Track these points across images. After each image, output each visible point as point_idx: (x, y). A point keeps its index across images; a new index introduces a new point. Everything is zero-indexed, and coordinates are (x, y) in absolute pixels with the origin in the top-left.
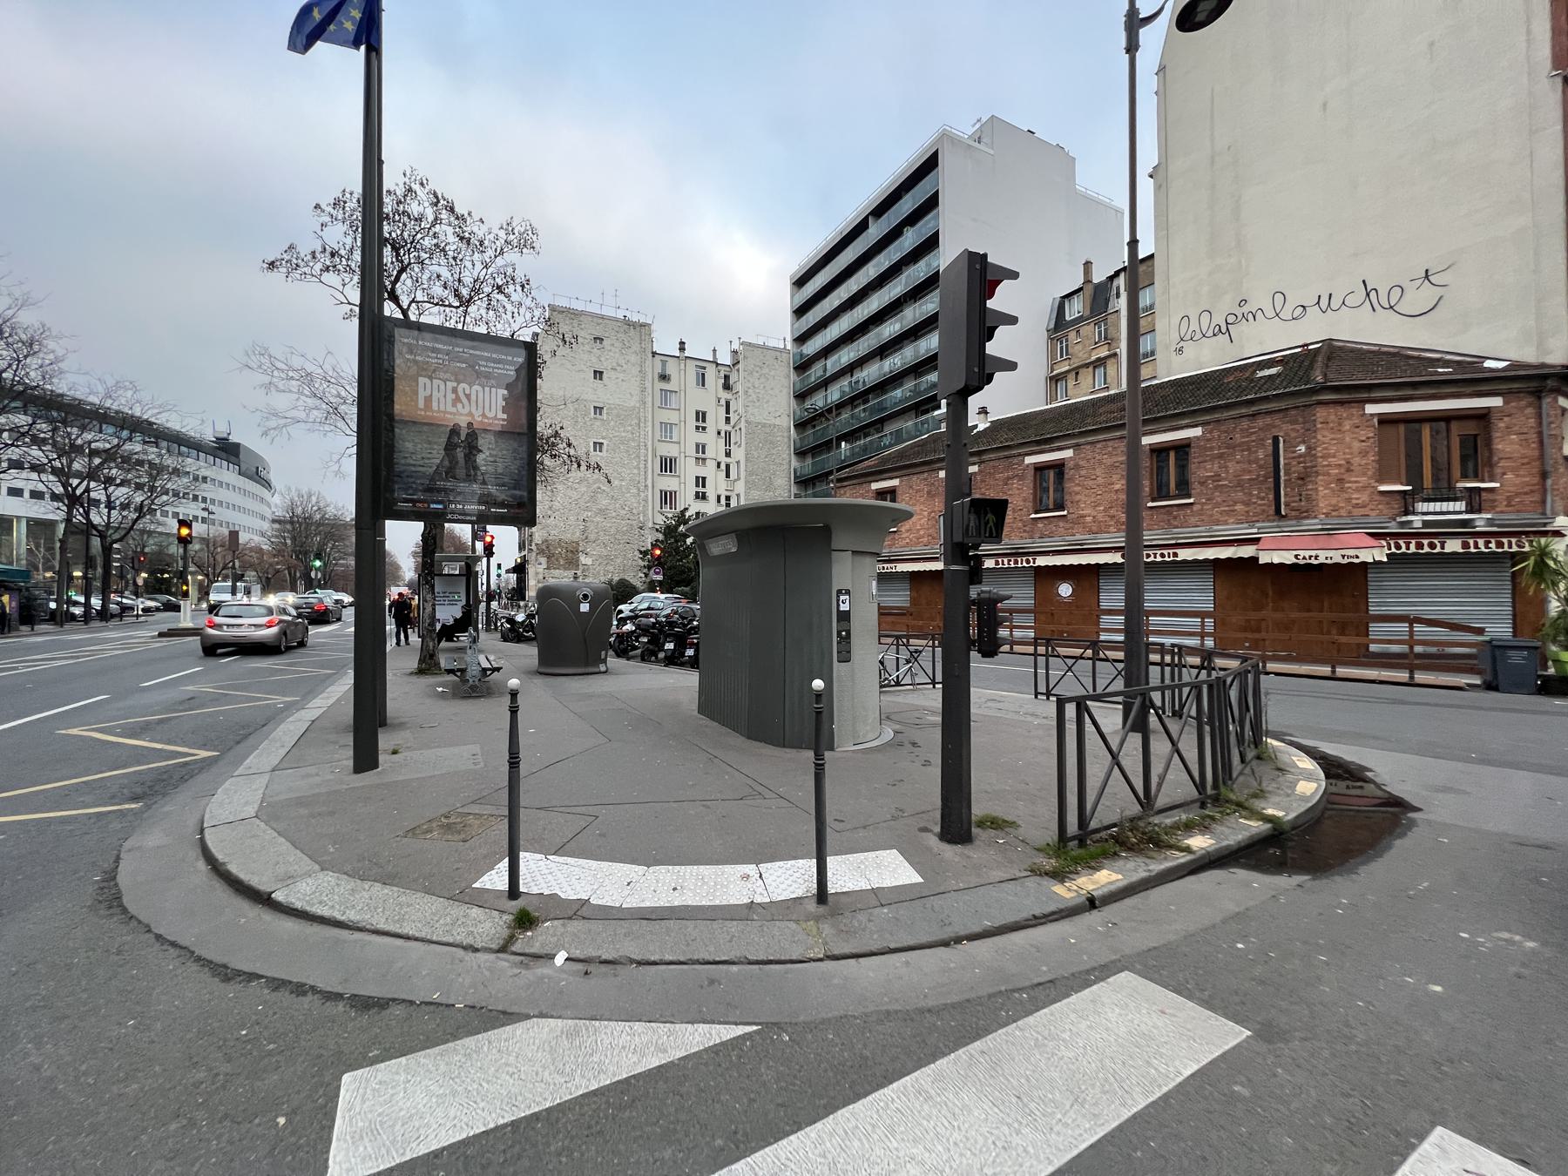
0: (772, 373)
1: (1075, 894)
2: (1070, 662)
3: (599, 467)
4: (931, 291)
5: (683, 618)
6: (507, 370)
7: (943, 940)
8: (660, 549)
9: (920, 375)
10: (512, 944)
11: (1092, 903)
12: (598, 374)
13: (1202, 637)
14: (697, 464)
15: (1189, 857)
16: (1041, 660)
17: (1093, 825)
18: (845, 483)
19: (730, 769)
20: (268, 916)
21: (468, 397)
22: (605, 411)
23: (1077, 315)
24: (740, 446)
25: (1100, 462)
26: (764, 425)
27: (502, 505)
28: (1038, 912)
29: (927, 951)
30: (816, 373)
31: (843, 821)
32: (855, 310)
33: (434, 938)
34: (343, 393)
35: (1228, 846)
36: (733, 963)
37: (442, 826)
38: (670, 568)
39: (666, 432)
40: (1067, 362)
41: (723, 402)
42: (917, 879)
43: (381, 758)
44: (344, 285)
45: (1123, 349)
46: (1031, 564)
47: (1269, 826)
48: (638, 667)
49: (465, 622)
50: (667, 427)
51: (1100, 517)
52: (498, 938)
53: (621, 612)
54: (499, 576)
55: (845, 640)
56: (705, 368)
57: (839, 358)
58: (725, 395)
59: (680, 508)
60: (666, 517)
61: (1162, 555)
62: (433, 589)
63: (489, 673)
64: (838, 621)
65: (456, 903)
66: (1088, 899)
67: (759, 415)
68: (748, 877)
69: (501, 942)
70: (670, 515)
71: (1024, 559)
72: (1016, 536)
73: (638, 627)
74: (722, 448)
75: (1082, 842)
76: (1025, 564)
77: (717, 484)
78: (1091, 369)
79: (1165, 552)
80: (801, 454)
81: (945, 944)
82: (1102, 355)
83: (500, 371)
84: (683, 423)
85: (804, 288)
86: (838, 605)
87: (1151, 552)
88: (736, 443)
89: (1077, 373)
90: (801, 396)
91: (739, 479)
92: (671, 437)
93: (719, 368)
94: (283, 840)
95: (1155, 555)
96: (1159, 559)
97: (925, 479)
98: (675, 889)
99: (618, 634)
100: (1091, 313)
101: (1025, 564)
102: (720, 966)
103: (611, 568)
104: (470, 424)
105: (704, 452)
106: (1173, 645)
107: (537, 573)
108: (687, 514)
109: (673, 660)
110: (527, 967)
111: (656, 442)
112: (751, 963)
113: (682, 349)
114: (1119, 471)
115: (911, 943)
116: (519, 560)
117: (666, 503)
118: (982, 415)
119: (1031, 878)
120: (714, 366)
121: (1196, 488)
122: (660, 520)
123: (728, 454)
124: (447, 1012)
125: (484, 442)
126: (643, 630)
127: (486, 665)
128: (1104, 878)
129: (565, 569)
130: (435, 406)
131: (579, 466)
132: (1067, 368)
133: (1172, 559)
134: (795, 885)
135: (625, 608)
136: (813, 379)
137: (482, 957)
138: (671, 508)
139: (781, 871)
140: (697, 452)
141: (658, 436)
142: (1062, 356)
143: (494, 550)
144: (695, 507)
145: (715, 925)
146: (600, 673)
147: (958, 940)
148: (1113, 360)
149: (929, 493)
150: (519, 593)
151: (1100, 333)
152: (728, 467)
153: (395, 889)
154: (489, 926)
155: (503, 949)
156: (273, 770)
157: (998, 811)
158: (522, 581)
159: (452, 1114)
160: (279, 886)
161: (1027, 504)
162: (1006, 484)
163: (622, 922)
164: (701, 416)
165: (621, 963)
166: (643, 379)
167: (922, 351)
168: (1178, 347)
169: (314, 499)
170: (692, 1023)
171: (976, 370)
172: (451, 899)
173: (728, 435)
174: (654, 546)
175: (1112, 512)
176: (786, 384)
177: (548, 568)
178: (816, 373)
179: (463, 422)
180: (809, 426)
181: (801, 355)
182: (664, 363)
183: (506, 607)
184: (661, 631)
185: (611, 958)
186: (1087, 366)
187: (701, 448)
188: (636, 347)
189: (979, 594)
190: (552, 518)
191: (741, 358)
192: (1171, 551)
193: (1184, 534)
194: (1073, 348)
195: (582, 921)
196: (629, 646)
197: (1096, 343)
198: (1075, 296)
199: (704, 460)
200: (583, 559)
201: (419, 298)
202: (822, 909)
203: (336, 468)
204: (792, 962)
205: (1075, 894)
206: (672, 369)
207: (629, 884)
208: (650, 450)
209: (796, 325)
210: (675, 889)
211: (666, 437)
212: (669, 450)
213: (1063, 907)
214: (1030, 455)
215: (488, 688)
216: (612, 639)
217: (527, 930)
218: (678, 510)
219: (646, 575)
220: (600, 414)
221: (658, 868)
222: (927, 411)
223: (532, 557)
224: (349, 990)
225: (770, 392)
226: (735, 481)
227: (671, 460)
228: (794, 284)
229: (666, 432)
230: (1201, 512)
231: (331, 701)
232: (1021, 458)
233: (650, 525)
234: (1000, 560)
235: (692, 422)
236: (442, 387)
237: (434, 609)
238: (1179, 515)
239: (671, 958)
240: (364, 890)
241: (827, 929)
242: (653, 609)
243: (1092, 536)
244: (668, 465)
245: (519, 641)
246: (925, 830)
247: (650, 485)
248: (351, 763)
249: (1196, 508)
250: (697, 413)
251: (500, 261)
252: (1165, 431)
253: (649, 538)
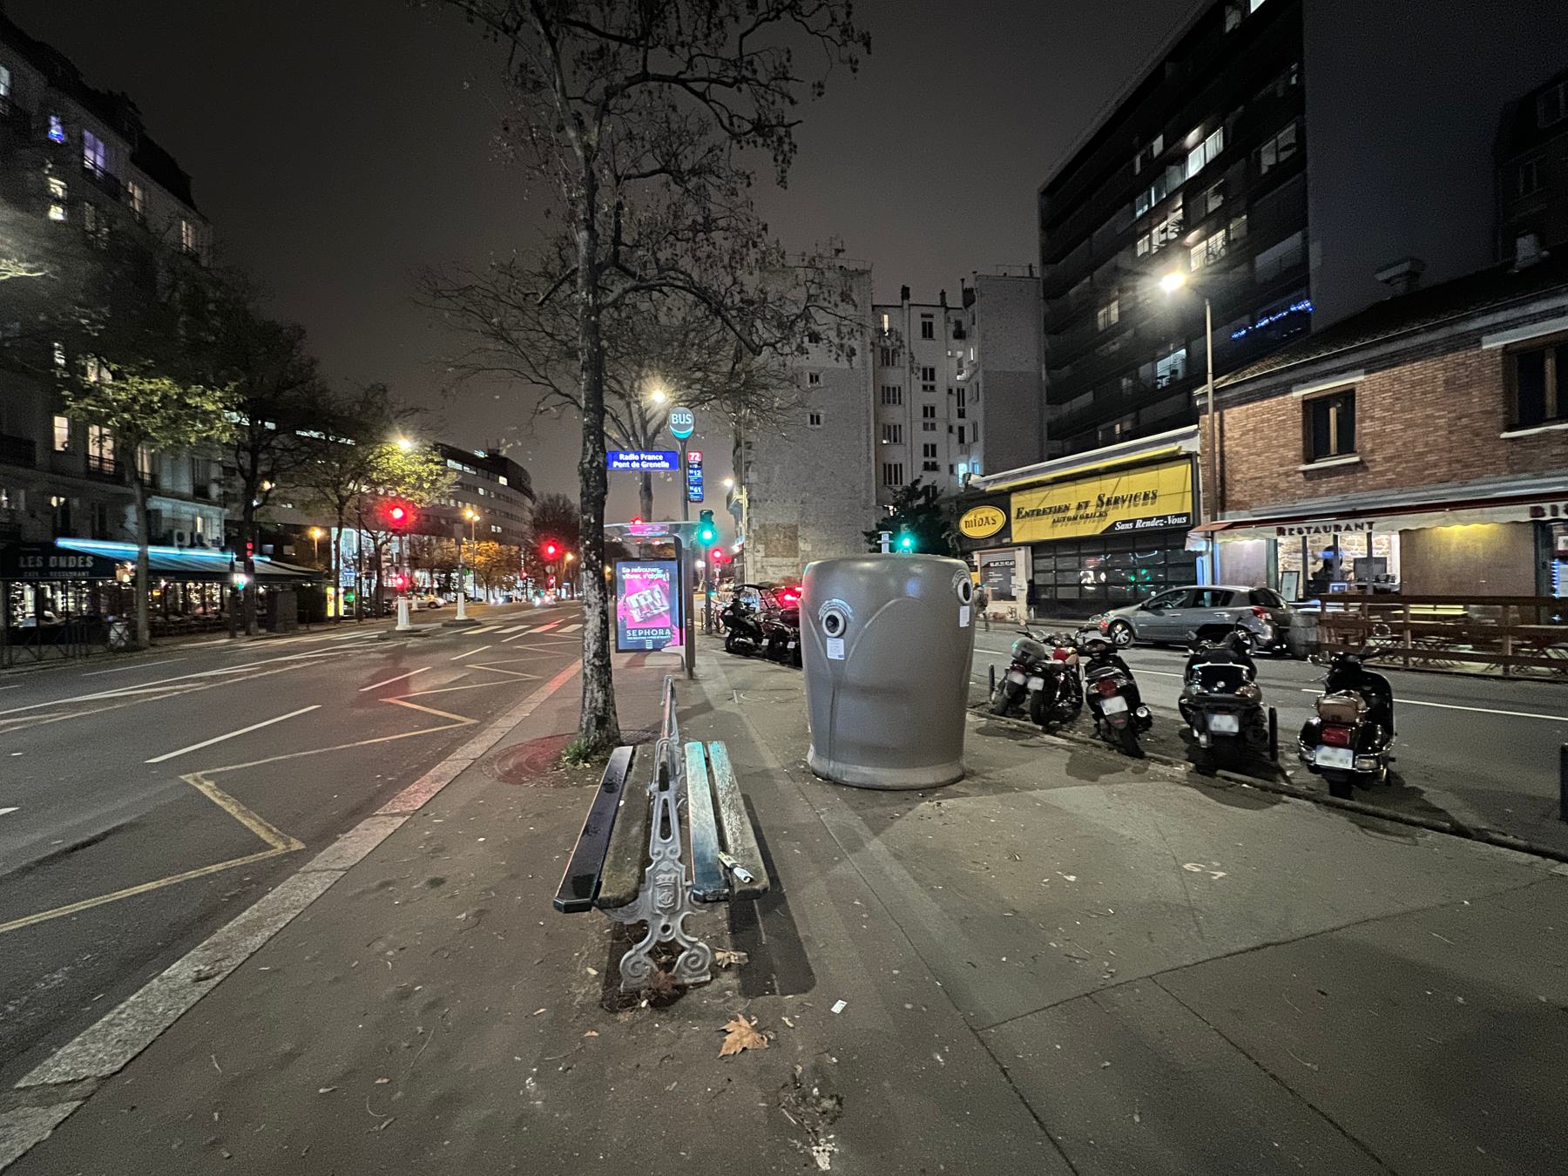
59: (907, 482)
120: (943, 309)
123: (961, 414)
169: (561, 503)
187: (929, 411)
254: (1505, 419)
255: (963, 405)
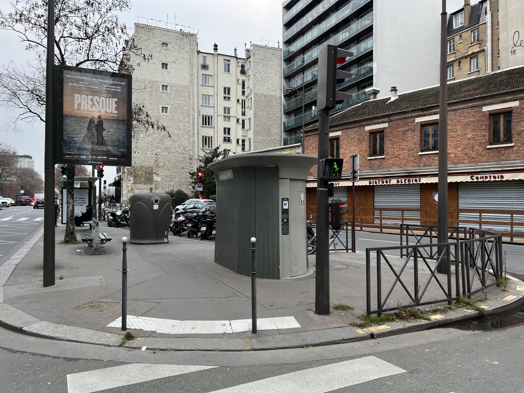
0: (270, 64)
1: (366, 332)
2: (419, 238)
3: (164, 129)
4: (368, 13)
5: (212, 213)
6: (117, 89)
7: (301, 345)
8: (202, 172)
9: (361, 64)
10: (125, 344)
11: (372, 336)
12: (165, 65)
13: (512, 226)
14: (225, 120)
15: (427, 322)
16: (404, 237)
17: (385, 308)
18: (309, 134)
19: (225, 286)
20: (22, 336)
21: (98, 103)
22: (169, 88)
23: (460, 26)
24: (251, 109)
25: (459, 121)
26: (265, 96)
27: (114, 156)
28: (345, 338)
29: (294, 349)
30: (297, 63)
31: (273, 306)
32: (322, 24)
33: (93, 342)
34: (19, 84)
35: (451, 319)
36: (213, 351)
37: (90, 306)
38: (208, 184)
39: (206, 100)
40: (453, 55)
41: (240, 82)
42: (298, 326)
43: (56, 281)
44: (26, 31)
45: (488, 46)
46: (418, 182)
47: (477, 312)
48: (186, 240)
49: (88, 216)
50: (207, 97)
51: (459, 154)
52: (119, 342)
53: (178, 210)
54: (105, 188)
55: (286, 223)
56: (229, 61)
57: (312, 54)
58: (241, 77)
59: (214, 147)
60: (206, 153)
61: (495, 177)
62: (73, 197)
63: (104, 242)
64: (282, 214)
65: (100, 332)
66: (370, 334)
67: (262, 90)
68: (225, 324)
69: (120, 344)
70: (208, 151)
71: (414, 179)
72: (410, 165)
73: (186, 218)
74: (240, 110)
75: (379, 314)
76: (414, 182)
77: (237, 133)
78: (468, 59)
79: (496, 175)
80: (288, 113)
81: (302, 347)
82: (475, 51)
83: (114, 90)
84: (216, 95)
85: (291, 10)
86: (282, 206)
87: (488, 175)
88: (248, 107)
89: (460, 62)
90: (288, 78)
91: (250, 129)
92: (209, 104)
93: (238, 60)
94: (20, 311)
95: (490, 177)
96: (492, 179)
97: (357, 132)
98: (192, 328)
99: (175, 222)
100: (469, 24)
101: (414, 182)
102: (208, 352)
103: (173, 183)
104: (99, 117)
105: (229, 113)
106: (470, 229)
107: (128, 187)
108: (219, 151)
109: (205, 237)
110: (131, 351)
111: (200, 107)
112: (220, 351)
113: (216, 49)
114: (471, 127)
115: (287, 346)
116: (117, 179)
117: (206, 144)
118: (393, 92)
119: (349, 327)
120: (235, 59)
121: (515, 137)
122: (202, 154)
123: (243, 114)
124: (102, 362)
125: (105, 125)
126: (189, 220)
127: (103, 237)
128: (384, 327)
129: (145, 184)
130: (82, 108)
131: (153, 127)
132: (478, 50)
133: (500, 179)
134: (244, 327)
135: (180, 207)
136: (296, 67)
137: (112, 348)
138: (209, 147)
139: (239, 323)
140: (225, 113)
141: (201, 103)
142: (450, 51)
143: (104, 173)
144: (224, 146)
145: (207, 339)
146: (164, 243)
147: (308, 346)
148: (482, 54)
149: (359, 139)
150: (117, 198)
151: (474, 37)
152: (243, 121)
153: (74, 327)
154: (116, 339)
155: (120, 346)
156: (4, 286)
157: (345, 302)
158: (118, 193)
159: (107, 383)
160: (24, 326)
161: (417, 146)
162: (404, 134)
163: (170, 338)
164: (227, 90)
165: (168, 350)
166: (192, 68)
167: (362, 49)
168: (513, 49)
170: (194, 365)
171: (331, 99)
172: (98, 330)
173: (244, 102)
174: (199, 170)
175: (466, 151)
176: (279, 70)
177: (134, 183)
178: (297, 63)
179: (96, 115)
180: (293, 96)
181: (289, 52)
182: (205, 58)
183: (109, 207)
184: (199, 220)
185: (164, 348)
186: (466, 57)
187: (227, 110)
188: (187, 48)
189: (332, 202)
190: (137, 153)
191: (251, 54)
192: (500, 175)
193: (507, 164)
194: (457, 46)
195: (153, 338)
196: (181, 229)
197: (472, 43)
198: (459, 14)
199: (229, 117)
200: (156, 178)
201: (65, 35)
202: (254, 335)
203: (13, 126)
204: (237, 351)
205: (366, 332)
206: (209, 61)
207: (173, 326)
208: (196, 111)
209: (286, 34)
210: (192, 328)
211: (206, 103)
212: (208, 112)
213: (358, 336)
214: (417, 117)
215: (104, 250)
216: (171, 225)
217: (130, 340)
218: (213, 148)
219: (194, 188)
220: (166, 90)
221: (186, 321)
222: (365, 87)
223: (125, 177)
224: (62, 356)
225: (270, 75)
226: (248, 130)
227: (209, 118)
228: (284, 8)
229: (206, 100)
230: (517, 152)
231: (23, 256)
232: (413, 119)
233: (196, 157)
234: (400, 180)
235: (221, 94)
236: (86, 98)
237: (73, 208)
238: (505, 153)
239: (188, 349)
240: (60, 327)
241: (254, 341)
242: (196, 208)
243: (454, 166)
244: (207, 121)
245: (117, 227)
246: (310, 310)
247: (196, 133)
248: (42, 283)
249: (515, 149)
250: (225, 89)
251: (109, 14)
252: (497, 103)
253: (195, 165)
254: (369, 153)
255: (245, 109)
